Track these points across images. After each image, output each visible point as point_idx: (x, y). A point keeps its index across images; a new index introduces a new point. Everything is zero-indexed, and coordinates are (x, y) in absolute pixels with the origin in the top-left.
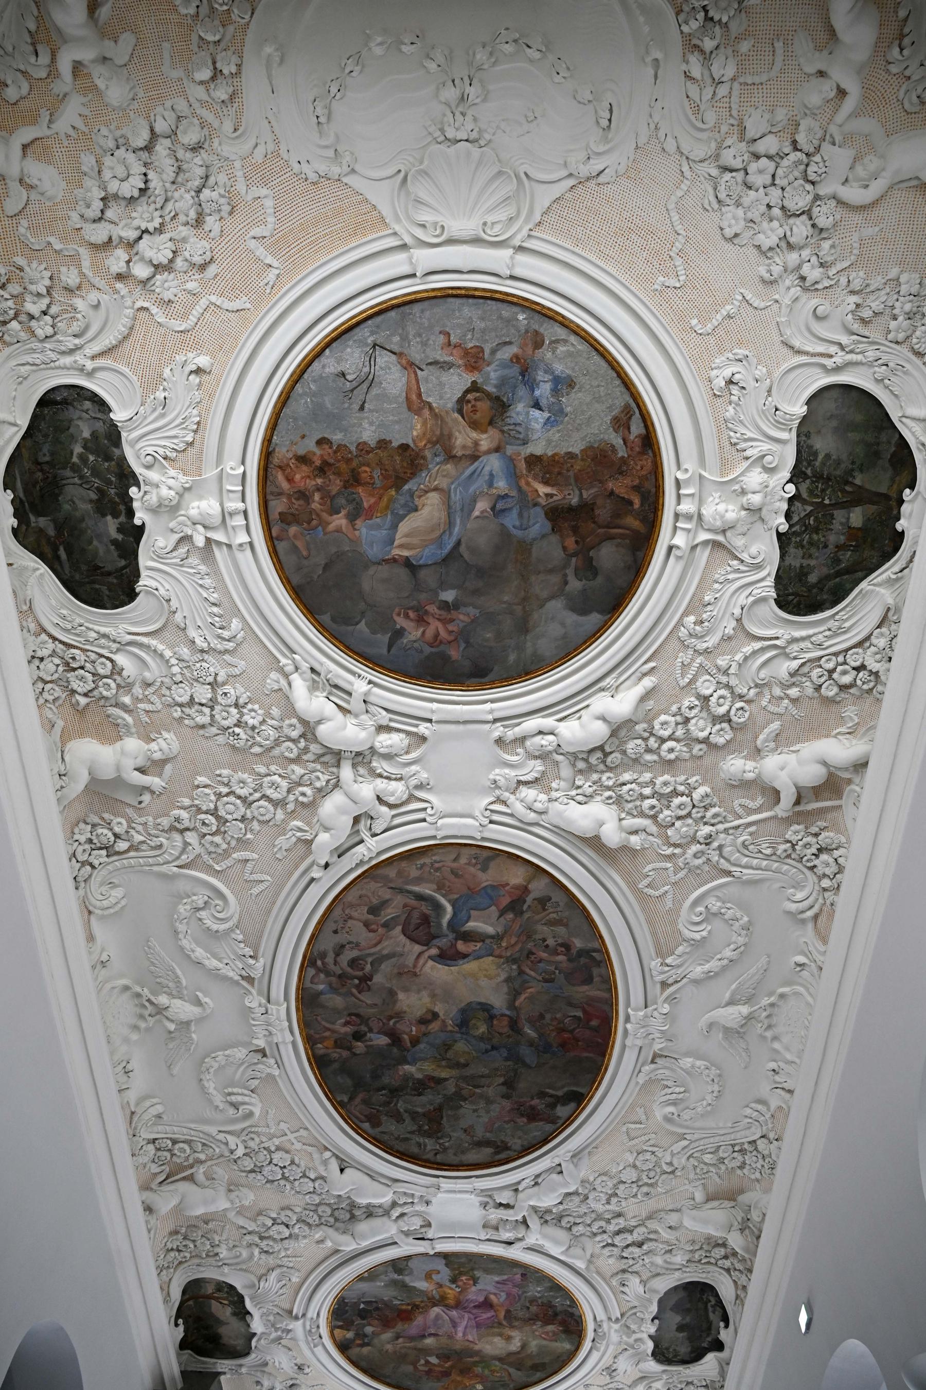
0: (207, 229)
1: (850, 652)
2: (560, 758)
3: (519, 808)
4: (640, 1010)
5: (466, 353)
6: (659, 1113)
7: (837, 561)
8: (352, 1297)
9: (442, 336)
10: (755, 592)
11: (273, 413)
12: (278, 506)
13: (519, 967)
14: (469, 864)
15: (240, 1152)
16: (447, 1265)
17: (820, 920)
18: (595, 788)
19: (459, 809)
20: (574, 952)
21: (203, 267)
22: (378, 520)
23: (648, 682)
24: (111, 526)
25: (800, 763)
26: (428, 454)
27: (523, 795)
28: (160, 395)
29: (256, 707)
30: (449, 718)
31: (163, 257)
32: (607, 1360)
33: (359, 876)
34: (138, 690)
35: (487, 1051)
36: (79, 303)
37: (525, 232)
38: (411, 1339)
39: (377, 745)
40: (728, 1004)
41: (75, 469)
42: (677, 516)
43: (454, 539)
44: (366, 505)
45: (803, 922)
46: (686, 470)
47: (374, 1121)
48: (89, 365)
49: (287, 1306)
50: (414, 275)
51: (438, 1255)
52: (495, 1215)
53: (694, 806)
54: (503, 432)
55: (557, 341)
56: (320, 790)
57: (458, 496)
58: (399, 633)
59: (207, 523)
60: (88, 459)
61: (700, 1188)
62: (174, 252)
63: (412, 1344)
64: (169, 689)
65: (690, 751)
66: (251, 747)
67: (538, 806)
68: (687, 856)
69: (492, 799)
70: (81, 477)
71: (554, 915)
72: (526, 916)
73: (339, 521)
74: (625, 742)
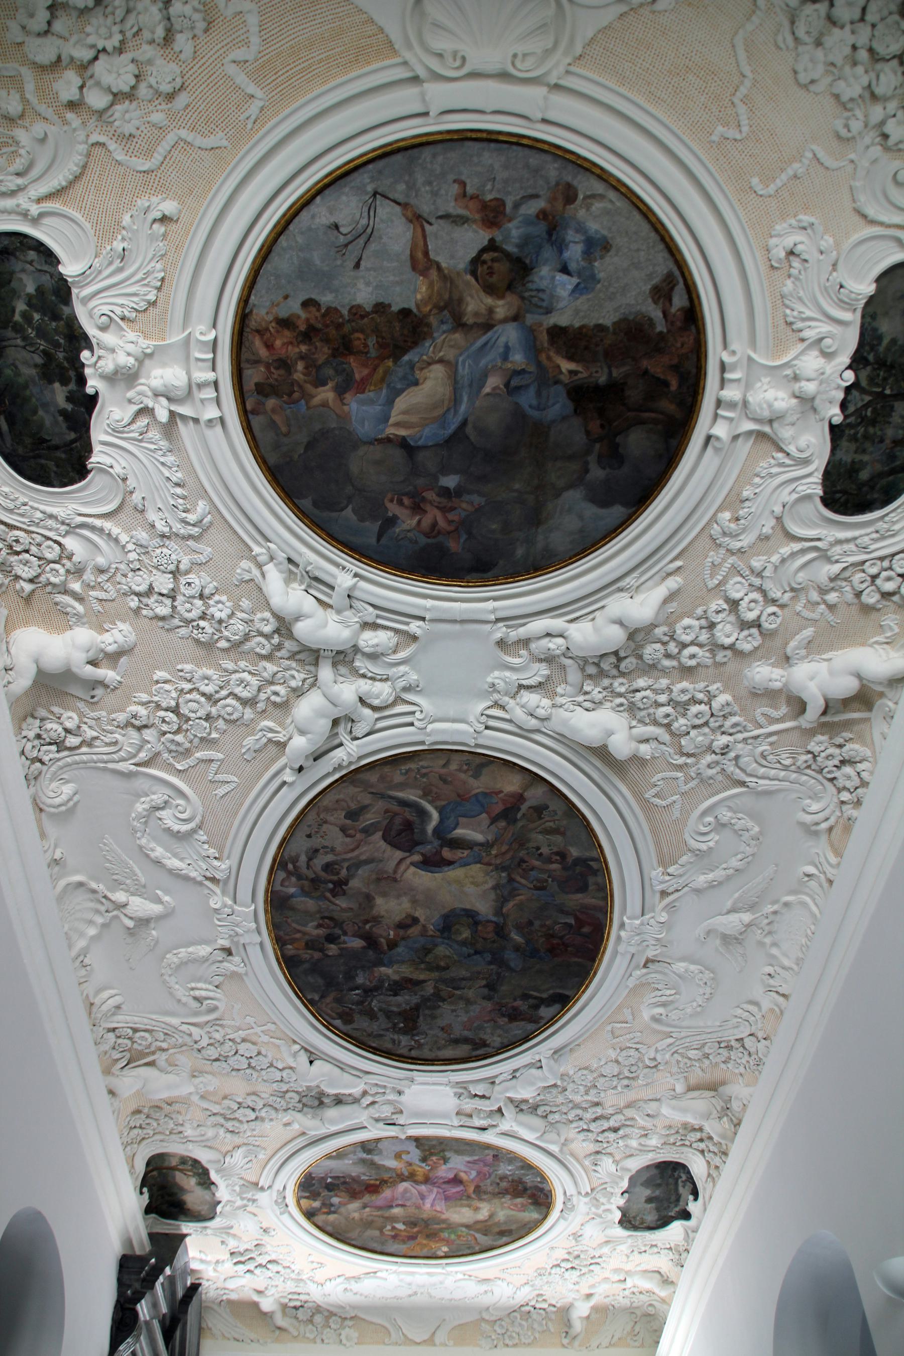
0: (177, 48)
1: (897, 557)
2: (568, 662)
3: (519, 714)
4: (637, 918)
5: (484, 206)
6: (646, 1014)
7: (892, 457)
8: (319, 1172)
9: (456, 186)
10: (800, 488)
11: (251, 269)
12: (254, 376)
13: (509, 875)
14: (460, 770)
15: (204, 1042)
16: (417, 1147)
17: (838, 832)
18: (605, 693)
19: (452, 714)
20: (570, 860)
21: (171, 97)
22: (371, 394)
23: (673, 583)
24: (59, 394)
25: (831, 673)
26: (433, 320)
27: (524, 700)
28: (119, 246)
29: (224, 598)
30: (444, 616)
31: (124, 82)
32: (574, 1227)
33: (336, 781)
34: (88, 576)
35: (469, 956)
36: (21, 135)
37: (562, 69)
38: (379, 1208)
39: (361, 643)
40: (729, 912)
41: (18, 328)
42: (719, 403)
43: (459, 419)
44: (357, 377)
45: (816, 834)
46: (734, 353)
47: (347, 1017)
48: (35, 210)
49: (254, 1179)
50: (426, 114)
51: (409, 1138)
52: (469, 1105)
53: (712, 715)
54: (523, 298)
55: (593, 196)
56: (294, 690)
57: (466, 371)
58: (391, 521)
59: (172, 395)
60: (32, 318)
61: (682, 1080)
62: (137, 77)
63: (379, 1213)
64: (125, 576)
65: (714, 656)
66: (217, 641)
67: (541, 712)
68: (699, 766)
69: (490, 703)
70: (25, 338)
71: (551, 824)
72: (520, 824)
73: (326, 394)
74: (642, 646)
